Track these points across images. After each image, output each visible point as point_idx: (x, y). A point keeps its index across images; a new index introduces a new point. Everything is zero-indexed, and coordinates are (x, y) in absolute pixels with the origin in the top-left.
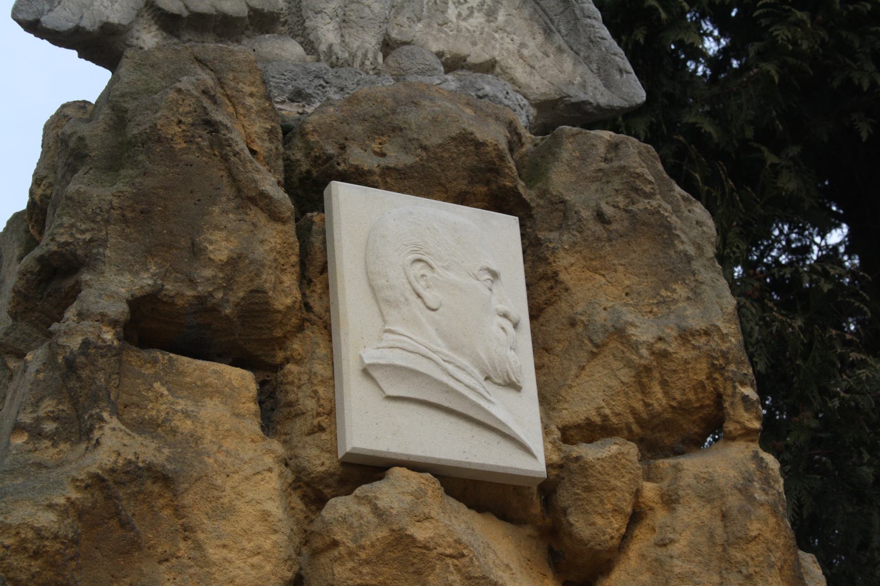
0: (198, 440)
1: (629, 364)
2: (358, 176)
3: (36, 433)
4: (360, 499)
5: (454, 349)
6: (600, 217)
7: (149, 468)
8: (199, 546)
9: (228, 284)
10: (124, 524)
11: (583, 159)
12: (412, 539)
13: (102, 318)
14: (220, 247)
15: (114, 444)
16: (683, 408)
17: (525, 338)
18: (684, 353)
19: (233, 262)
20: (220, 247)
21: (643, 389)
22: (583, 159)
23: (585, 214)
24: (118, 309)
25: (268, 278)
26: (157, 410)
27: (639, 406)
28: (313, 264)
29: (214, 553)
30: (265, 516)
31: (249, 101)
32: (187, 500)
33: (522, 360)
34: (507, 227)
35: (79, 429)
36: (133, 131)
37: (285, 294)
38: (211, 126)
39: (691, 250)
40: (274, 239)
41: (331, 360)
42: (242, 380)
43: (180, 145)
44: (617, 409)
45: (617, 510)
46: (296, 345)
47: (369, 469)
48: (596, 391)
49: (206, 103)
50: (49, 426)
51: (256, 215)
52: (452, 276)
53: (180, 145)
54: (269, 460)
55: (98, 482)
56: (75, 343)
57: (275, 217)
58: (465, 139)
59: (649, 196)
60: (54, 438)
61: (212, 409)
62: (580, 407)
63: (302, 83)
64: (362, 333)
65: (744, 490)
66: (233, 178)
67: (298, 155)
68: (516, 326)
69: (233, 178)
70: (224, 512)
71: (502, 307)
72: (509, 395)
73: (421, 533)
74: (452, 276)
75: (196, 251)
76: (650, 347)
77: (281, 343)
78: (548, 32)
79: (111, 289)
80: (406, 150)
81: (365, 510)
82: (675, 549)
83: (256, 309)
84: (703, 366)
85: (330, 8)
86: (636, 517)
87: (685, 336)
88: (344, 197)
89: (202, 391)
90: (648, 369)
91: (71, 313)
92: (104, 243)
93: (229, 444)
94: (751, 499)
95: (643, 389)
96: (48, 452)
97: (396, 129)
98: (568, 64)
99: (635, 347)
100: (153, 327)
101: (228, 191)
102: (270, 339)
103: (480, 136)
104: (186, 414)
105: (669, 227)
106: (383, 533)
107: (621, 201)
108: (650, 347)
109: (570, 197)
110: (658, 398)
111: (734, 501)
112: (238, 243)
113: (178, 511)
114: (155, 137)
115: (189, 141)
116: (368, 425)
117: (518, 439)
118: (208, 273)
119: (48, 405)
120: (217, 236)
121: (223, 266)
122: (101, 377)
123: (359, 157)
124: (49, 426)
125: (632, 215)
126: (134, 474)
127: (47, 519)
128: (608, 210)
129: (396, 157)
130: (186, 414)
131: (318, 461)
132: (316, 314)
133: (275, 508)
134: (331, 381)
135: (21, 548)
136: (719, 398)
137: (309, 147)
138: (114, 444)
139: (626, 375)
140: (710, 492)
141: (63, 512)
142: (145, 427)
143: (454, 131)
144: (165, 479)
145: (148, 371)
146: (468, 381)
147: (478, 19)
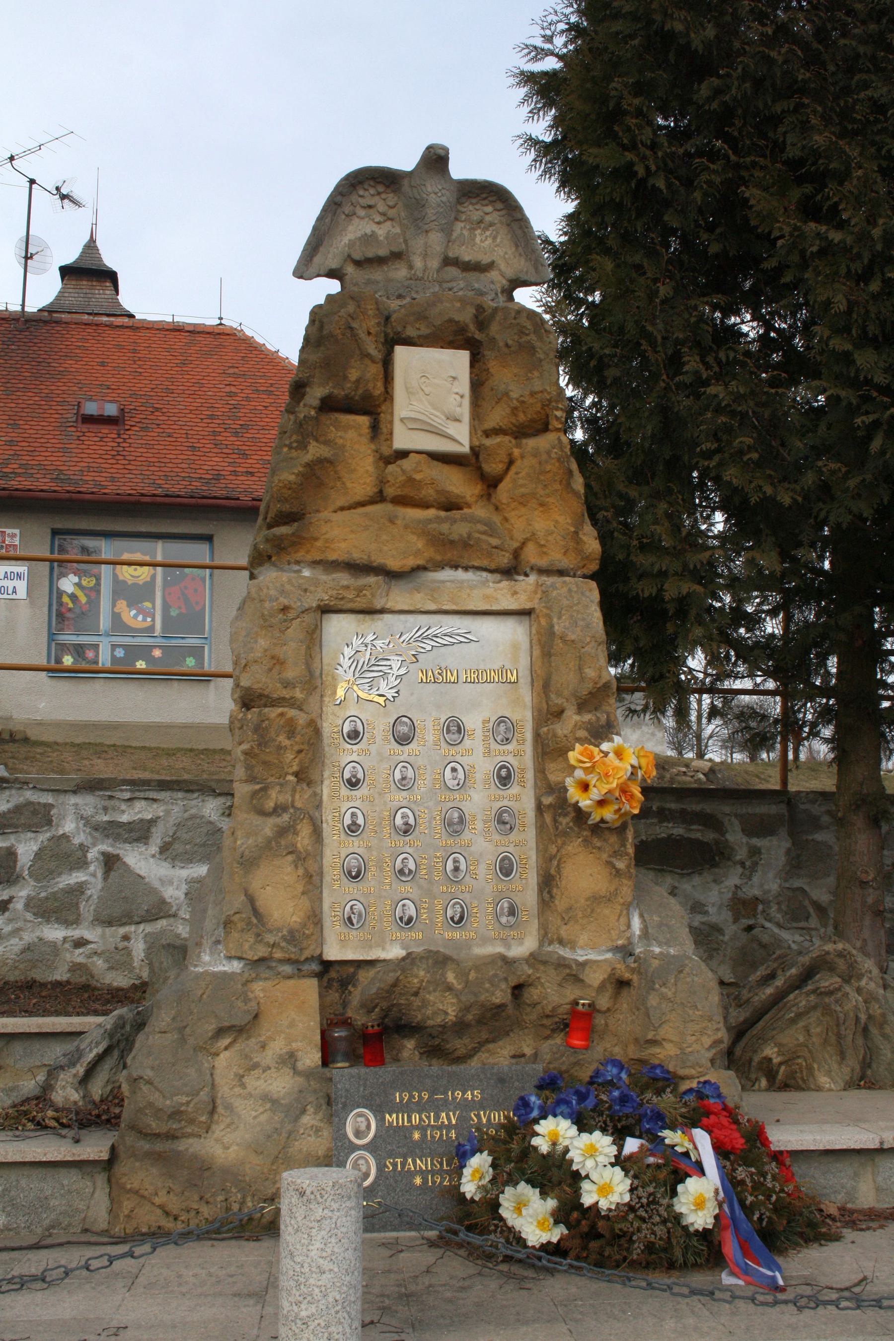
0: (344, 446)
1: (509, 406)
2: (408, 342)
3: (290, 447)
4: (399, 466)
5: (435, 409)
6: (507, 345)
7: (325, 458)
8: (343, 483)
9: (357, 388)
10: (318, 478)
11: (505, 319)
12: (415, 480)
13: (311, 406)
14: (353, 375)
15: (315, 450)
16: (533, 421)
17: (466, 402)
18: (531, 401)
19: (358, 381)
20: (353, 375)
21: (515, 415)
22: (505, 319)
23: (501, 344)
24: (316, 403)
25: (371, 385)
26: (331, 436)
27: (514, 421)
28: (388, 377)
29: (349, 485)
30: (367, 471)
31: (370, 312)
32: (339, 468)
33: (465, 411)
34: (464, 356)
35: (303, 446)
36: (325, 332)
37: (378, 389)
38: (351, 329)
39: (542, 356)
40: (374, 370)
41: (392, 414)
42: (364, 421)
43: (340, 337)
44: (504, 424)
45: (501, 462)
46: (383, 408)
47: (403, 454)
48: (497, 417)
49: (350, 319)
50: (295, 445)
51: (367, 361)
52: (436, 381)
53: (340, 337)
54: (369, 452)
55: (308, 465)
56: (302, 416)
57: (374, 362)
58: (451, 321)
59: (527, 335)
60: (296, 449)
61: (351, 434)
62: (490, 424)
63: (401, 291)
64: (405, 405)
65: (548, 453)
66: (360, 349)
67: (389, 331)
68: (462, 397)
69: (360, 349)
70: (353, 471)
71: (456, 390)
72: (457, 424)
73: (418, 477)
74: (436, 381)
75: (345, 378)
76: (517, 400)
77: (379, 406)
78: (517, 246)
79: (316, 393)
80: (428, 327)
81: (398, 470)
82: (520, 475)
83: (367, 396)
84: (539, 405)
85: (418, 252)
86: (511, 463)
87: (532, 394)
88: (401, 352)
89: (347, 428)
90: (516, 408)
91: (302, 404)
92: (313, 377)
93: (356, 447)
94: (550, 457)
95: (515, 415)
96: (294, 454)
97: (425, 318)
98: (523, 261)
99: (511, 399)
100: (328, 405)
101: (358, 352)
102: (373, 406)
103: (457, 319)
104: (341, 437)
105: (533, 348)
106: (404, 478)
107: (516, 337)
108: (517, 400)
109: (497, 337)
110: (522, 418)
111: (544, 457)
112: (360, 373)
113: (336, 472)
114: (331, 335)
115: (343, 335)
116: (402, 439)
117: (460, 438)
118: (349, 385)
119: (294, 437)
120: (353, 371)
121: (354, 382)
122: (310, 428)
123: (411, 332)
124: (295, 445)
125: (520, 344)
126: (321, 462)
127: (292, 478)
128: (510, 342)
129: (425, 331)
130: (341, 437)
131: (386, 451)
132: (388, 395)
133: (371, 469)
134: (391, 422)
135: (285, 486)
136: (547, 416)
137: (393, 328)
138: (315, 450)
139: (508, 410)
140: (536, 454)
141: (297, 475)
142: (327, 443)
143: (446, 318)
144: (331, 462)
145: (328, 422)
146: (439, 420)
147: (489, 241)
